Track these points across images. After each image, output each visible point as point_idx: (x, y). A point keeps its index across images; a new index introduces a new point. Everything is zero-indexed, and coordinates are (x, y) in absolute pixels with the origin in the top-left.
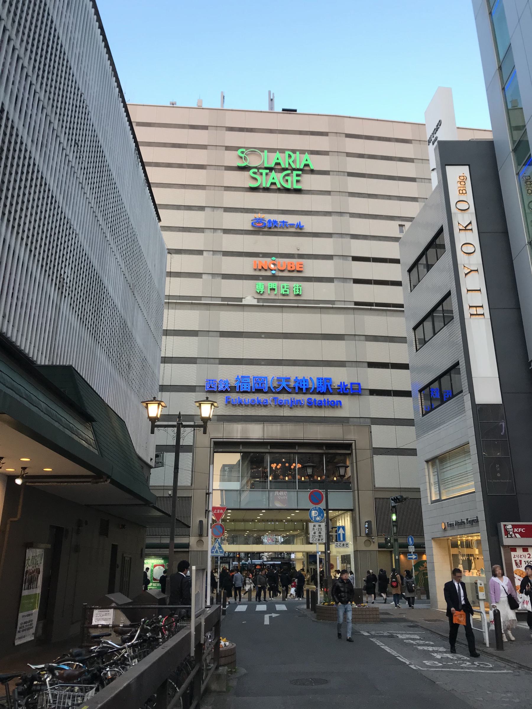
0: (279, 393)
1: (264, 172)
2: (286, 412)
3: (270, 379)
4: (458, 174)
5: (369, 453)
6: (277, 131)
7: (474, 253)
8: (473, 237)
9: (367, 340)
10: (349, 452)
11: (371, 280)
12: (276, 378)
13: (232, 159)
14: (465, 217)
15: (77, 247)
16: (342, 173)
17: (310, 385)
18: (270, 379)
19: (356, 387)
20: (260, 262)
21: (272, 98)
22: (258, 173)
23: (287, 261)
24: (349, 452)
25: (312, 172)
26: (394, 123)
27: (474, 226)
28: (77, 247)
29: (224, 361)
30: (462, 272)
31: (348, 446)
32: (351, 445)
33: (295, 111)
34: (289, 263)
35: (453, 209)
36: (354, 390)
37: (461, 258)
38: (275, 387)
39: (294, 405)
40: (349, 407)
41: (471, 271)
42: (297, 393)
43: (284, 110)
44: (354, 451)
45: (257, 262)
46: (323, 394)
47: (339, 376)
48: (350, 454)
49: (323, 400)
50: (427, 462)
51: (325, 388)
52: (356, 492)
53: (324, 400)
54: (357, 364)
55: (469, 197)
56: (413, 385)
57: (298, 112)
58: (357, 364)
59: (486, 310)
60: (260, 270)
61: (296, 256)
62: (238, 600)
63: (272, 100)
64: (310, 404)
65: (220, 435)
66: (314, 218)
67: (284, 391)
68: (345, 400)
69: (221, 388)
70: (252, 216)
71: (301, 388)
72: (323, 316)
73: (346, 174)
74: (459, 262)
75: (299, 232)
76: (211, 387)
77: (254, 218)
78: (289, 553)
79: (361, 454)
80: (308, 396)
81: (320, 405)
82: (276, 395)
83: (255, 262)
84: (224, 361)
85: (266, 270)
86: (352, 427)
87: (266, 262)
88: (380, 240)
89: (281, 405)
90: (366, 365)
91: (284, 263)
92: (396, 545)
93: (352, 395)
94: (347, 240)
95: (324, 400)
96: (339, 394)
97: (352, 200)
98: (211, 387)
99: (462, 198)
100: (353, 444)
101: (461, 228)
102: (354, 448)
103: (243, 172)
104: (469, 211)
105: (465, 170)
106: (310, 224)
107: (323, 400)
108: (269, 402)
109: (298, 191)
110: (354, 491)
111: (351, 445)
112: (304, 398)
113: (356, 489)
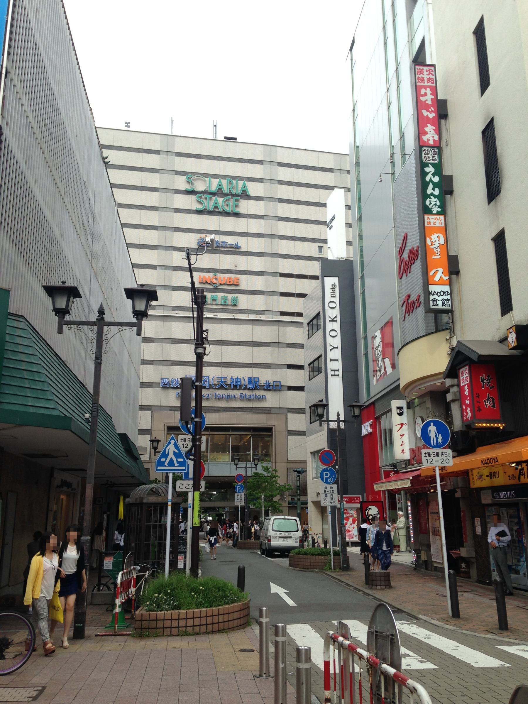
0: (218, 389)
1: (208, 196)
2: (224, 404)
3: (211, 378)
4: (331, 282)
5: (285, 434)
6: (220, 158)
7: (335, 338)
8: (337, 326)
9: (287, 347)
10: (270, 434)
11: (294, 294)
12: (215, 377)
13: (180, 183)
14: (333, 312)
15: (11, 194)
16: (274, 200)
17: (243, 382)
18: (211, 378)
19: (278, 384)
20: (204, 277)
21: (215, 124)
22: (203, 197)
23: (227, 276)
24: (270, 434)
25: (249, 198)
26: (320, 153)
27: (338, 319)
28: (11, 194)
29: (175, 363)
30: (329, 348)
31: (270, 430)
32: (271, 428)
33: (235, 139)
34: (228, 278)
35: (327, 307)
36: (275, 387)
37: (329, 340)
38: (215, 384)
39: (229, 399)
40: (272, 400)
41: (334, 348)
42: (232, 389)
43: (226, 138)
44: (274, 433)
45: (202, 277)
46: (252, 390)
47: (265, 376)
48: (271, 435)
49: (252, 394)
50: (311, 453)
51: (254, 385)
52: (274, 463)
53: (253, 395)
54: (279, 366)
55: (337, 300)
56: (306, 402)
57: (238, 140)
58: (279, 366)
59: (340, 373)
60: (204, 283)
61: (234, 272)
62: (452, 334)
63: (215, 126)
64: (242, 398)
65: (172, 422)
66: (250, 239)
67: (222, 387)
68: (269, 395)
69: (173, 385)
70: (198, 236)
71: (236, 385)
72: (254, 327)
73: (277, 200)
74: (327, 342)
75: (236, 250)
76: (165, 384)
77: (199, 238)
78: (185, 553)
79: (278, 439)
80: (241, 392)
81: (249, 400)
82: (216, 391)
83: (200, 276)
84: (175, 363)
85: (209, 284)
86: (273, 415)
87: (209, 277)
88: (302, 259)
89: (219, 399)
90: (286, 366)
91: (224, 278)
92: (299, 503)
93: (275, 390)
94: (275, 259)
95: (253, 395)
96: (265, 390)
97: (281, 224)
98: (165, 384)
99: (333, 299)
100: (274, 429)
101: (330, 320)
102: (273, 431)
103: (190, 196)
104: (336, 309)
105: (335, 280)
106: (246, 244)
107: (252, 394)
108: (210, 396)
109: (237, 215)
110: (272, 463)
111: (271, 428)
112: (237, 393)
113: (274, 461)
